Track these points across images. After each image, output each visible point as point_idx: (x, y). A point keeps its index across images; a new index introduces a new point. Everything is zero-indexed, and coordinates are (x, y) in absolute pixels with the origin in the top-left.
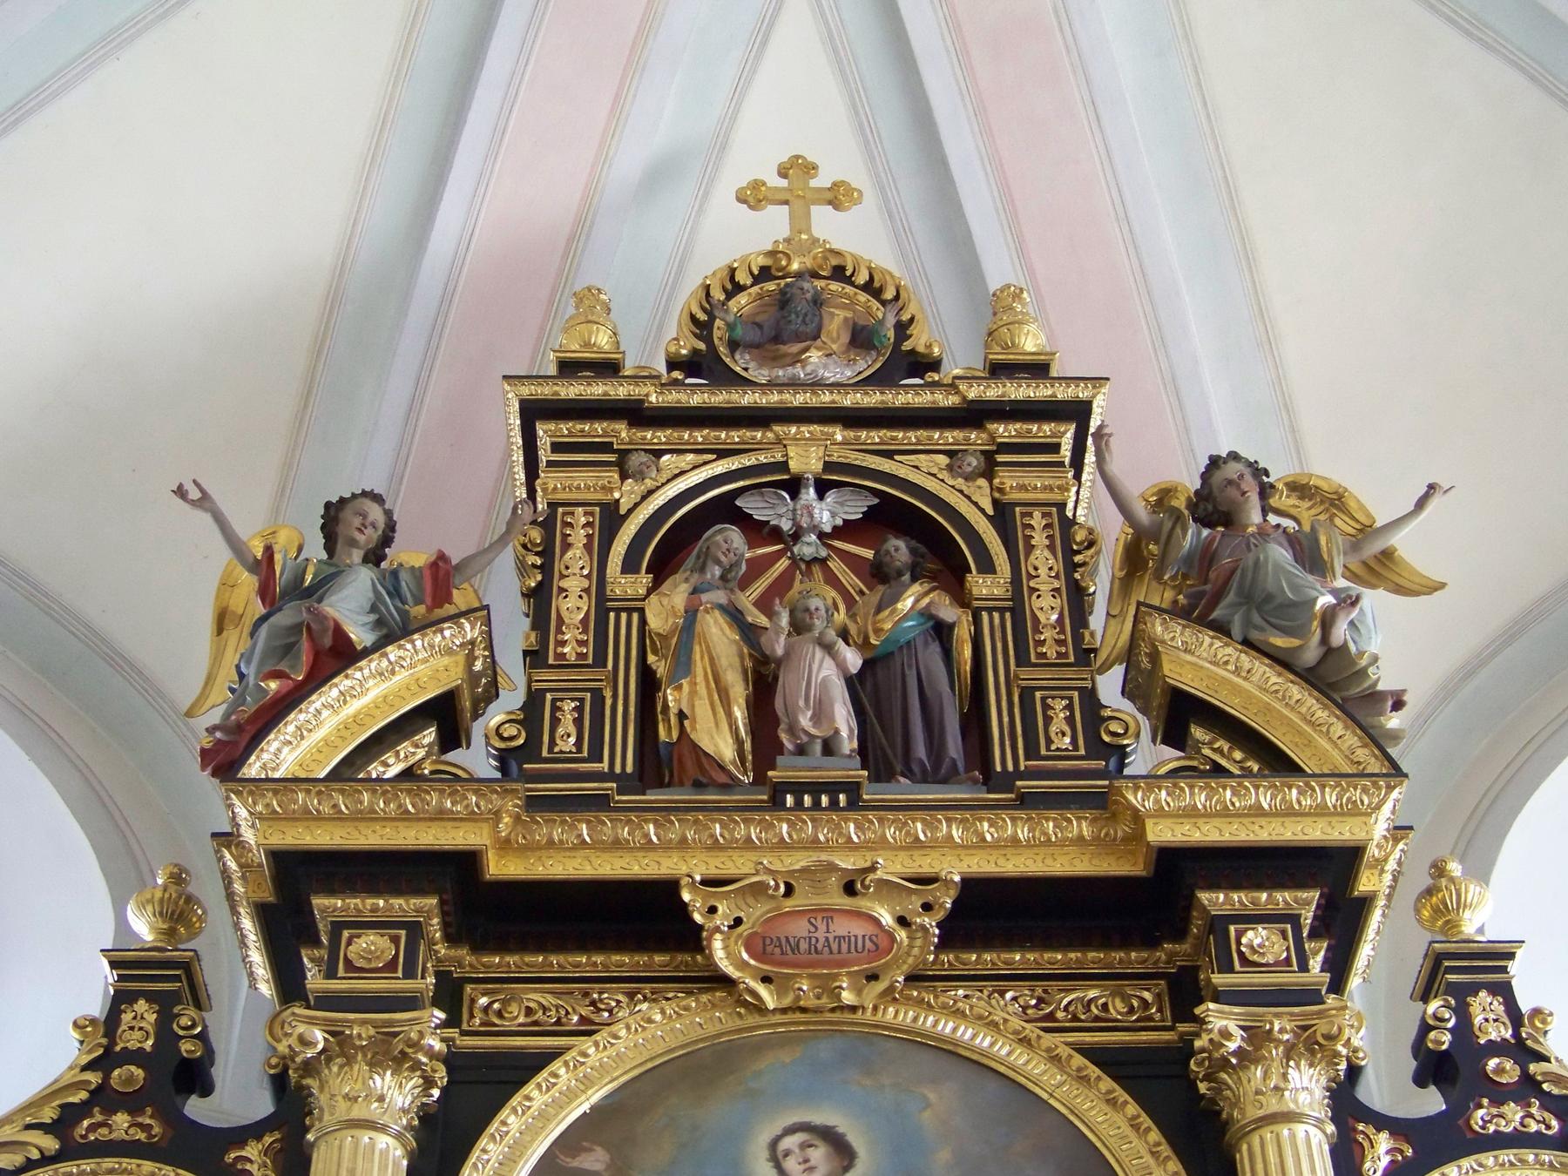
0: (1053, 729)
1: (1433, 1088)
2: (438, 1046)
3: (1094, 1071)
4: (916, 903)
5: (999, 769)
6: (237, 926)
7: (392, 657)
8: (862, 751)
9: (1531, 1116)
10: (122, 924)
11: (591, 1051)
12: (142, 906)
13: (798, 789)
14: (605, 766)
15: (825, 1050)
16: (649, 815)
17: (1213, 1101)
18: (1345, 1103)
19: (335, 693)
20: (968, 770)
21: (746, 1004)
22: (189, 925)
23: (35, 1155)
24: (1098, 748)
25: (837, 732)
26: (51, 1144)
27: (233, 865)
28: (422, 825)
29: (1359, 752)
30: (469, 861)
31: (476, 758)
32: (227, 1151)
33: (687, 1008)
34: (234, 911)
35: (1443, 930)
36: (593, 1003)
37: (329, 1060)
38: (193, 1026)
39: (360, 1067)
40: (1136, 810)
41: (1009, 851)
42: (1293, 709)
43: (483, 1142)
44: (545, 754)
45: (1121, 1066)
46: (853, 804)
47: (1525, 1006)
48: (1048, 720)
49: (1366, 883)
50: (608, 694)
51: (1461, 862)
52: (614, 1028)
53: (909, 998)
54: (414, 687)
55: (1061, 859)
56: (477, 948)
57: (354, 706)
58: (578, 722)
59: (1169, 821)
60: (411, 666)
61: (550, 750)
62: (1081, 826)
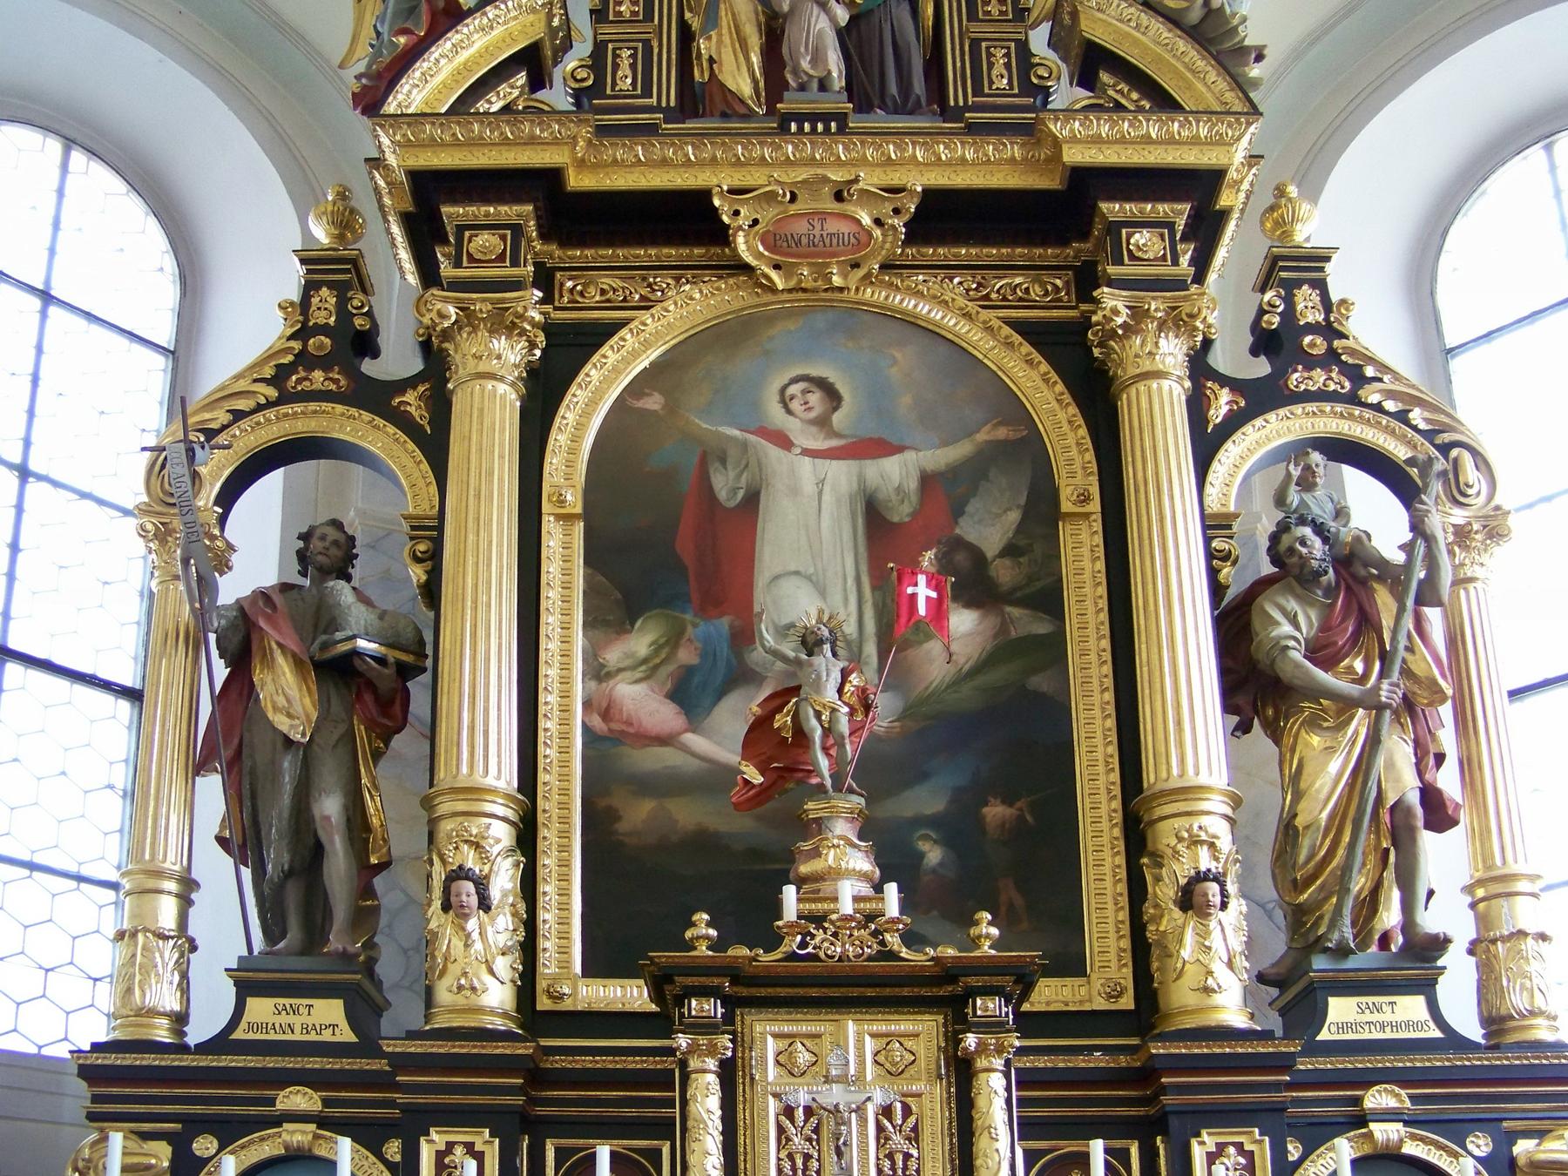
0: (995, 72)
1: (1263, 358)
2: (538, 317)
3: (1017, 338)
4: (889, 208)
5: (952, 103)
6: (388, 232)
7: (491, 16)
8: (849, 88)
9: (1331, 378)
10: (306, 233)
11: (649, 321)
12: (318, 217)
13: (800, 118)
14: (654, 100)
15: (820, 321)
16: (688, 139)
17: (1103, 362)
18: (1199, 366)
19: (448, 45)
20: (929, 103)
21: (761, 286)
22: (354, 231)
23: (263, 401)
24: (1028, 88)
25: (829, 72)
26: (272, 393)
27: (382, 183)
28: (520, 148)
29: (1228, 95)
30: (553, 176)
31: (558, 96)
32: (392, 398)
33: (719, 289)
34: (386, 221)
35: (1280, 238)
36: (650, 285)
37: (460, 329)
38: (362, 307)
39: (483, 333)
40: (1056, 137)
41: (959, 168)
42: (1179, 59)
43: (573, 388)
44: (609, 92)
45: (1038, 335)
46: (842, 130)
47: (1335, 297)
48: (991, 66)
49: (1225, 199)
50: (655, 44)
51: (1298, 186)
52: (665, 304)
53: (883, 281)
54: (508, 40)
55: (1000, 175)
56: (564, 244)
57: (464, 55)
58: (633, 66)
59: (1079, 147)
60: (505, 23)
61: (613, 89)
62: (1014, 149)
